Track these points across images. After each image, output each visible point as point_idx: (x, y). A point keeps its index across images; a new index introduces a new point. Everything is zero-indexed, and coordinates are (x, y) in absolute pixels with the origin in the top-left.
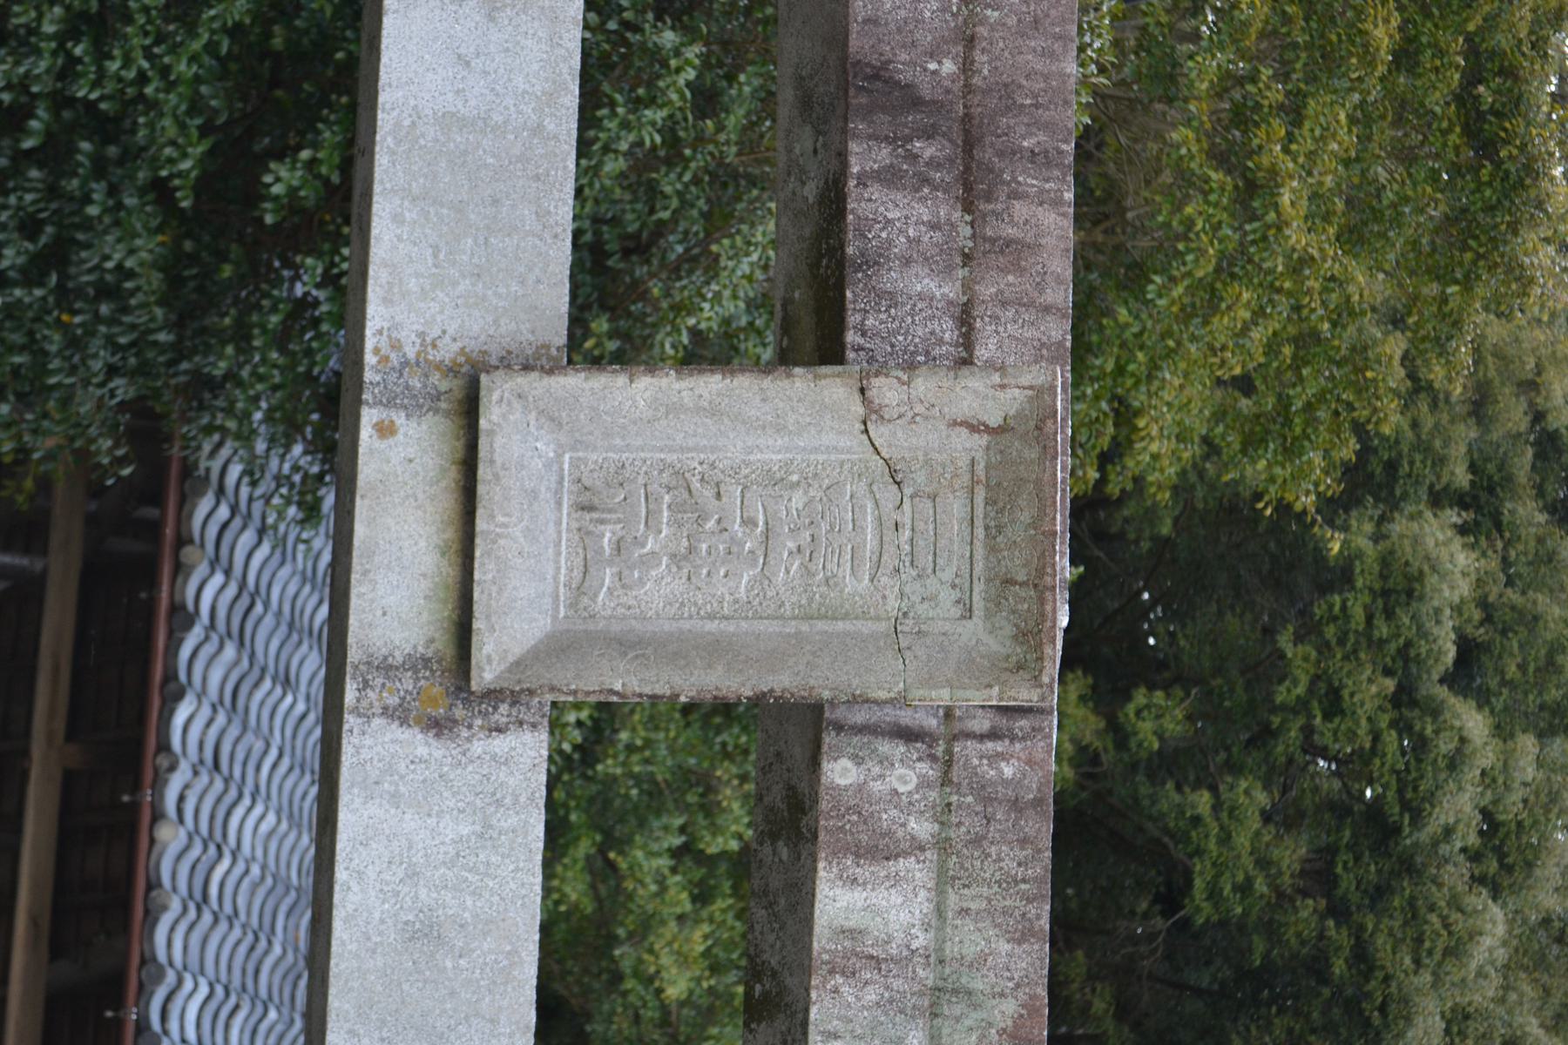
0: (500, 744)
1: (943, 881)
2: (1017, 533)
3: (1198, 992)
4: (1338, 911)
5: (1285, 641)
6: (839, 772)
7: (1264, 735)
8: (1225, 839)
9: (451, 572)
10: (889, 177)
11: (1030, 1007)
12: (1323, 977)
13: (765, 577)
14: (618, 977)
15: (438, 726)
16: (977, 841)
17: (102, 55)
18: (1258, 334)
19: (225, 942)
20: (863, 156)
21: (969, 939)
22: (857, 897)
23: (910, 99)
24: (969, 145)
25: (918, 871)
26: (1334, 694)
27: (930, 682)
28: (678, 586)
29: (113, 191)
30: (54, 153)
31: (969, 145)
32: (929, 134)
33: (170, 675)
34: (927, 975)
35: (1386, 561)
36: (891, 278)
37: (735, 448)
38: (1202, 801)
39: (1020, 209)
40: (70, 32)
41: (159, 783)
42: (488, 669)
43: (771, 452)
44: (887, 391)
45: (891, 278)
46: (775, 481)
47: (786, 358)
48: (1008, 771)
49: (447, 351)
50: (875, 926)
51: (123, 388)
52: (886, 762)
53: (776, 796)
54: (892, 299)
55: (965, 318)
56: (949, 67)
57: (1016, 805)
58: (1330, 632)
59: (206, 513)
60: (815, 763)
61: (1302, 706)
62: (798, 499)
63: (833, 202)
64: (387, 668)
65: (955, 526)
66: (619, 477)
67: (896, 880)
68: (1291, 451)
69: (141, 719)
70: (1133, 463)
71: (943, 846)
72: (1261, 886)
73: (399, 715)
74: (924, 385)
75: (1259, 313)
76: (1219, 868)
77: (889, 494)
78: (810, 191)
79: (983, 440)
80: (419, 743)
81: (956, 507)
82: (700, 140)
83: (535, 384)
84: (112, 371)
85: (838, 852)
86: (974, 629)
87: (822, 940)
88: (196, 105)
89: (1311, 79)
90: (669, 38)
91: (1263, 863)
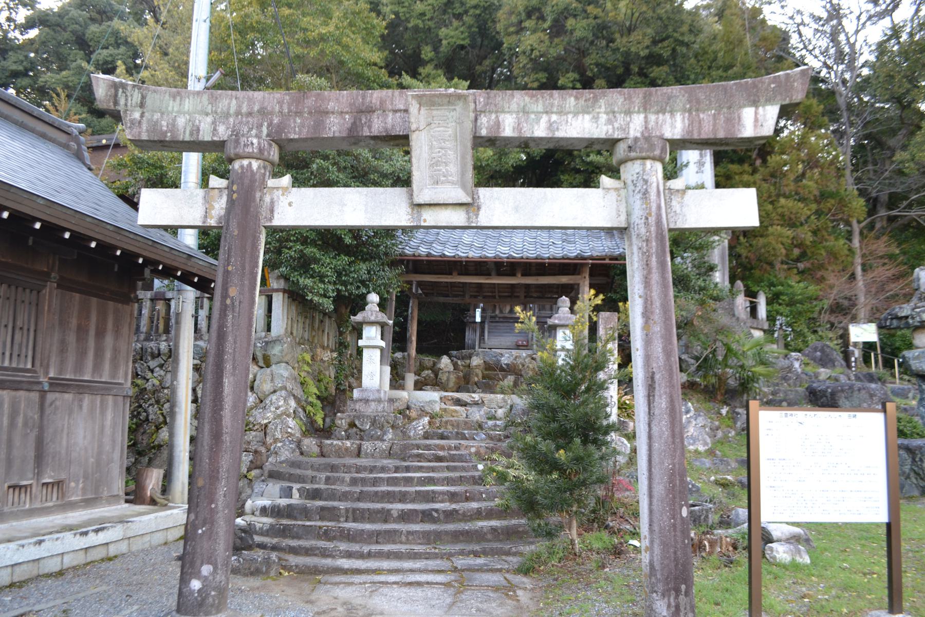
0: (481, 197)
1: (503, 112)
2: (440, 100)
3: (482, 41)
4: (466, 12)
5: (410, 25)
6: (484, 132)
7: (429, 29)
8: (452, 37)
9: (450, 208)
10: (370, 127)
11: (526, 94)
12: (480, 15)
13: (449, 149)
14: (488, 165)
15: (479, 208)
16: (496, 105)
17: (327, 276)
18: (352, 36)
19: (490, 243)
20: (366, 133)
21: (514, 106)
22: (507, 128)
23: (354, 124)
24: (362, 112)
25: (502, 116)
26: (421, 14)
27: (468, 117)
28: (451, 165)
29: (351, 272)
30: (344, 284)
31: (362, 112)
32: (361, 120)
33: (440, 256)
34: (521, 114)
35: (392, 4)
36: (389, 126)
37: (425, 155)
38: (444, 42)
39: (374, 101)
40: (323, 282)
41: (461, 257)
42: (469, 200)
43: (426, 148)
44: (414, 127)
45: (389, 126)
46: (431, 147)
47: (408, 145)
48: (482, 100)
49: (410, 210)
50: (512, 125)
51: (387, 268)
52: (481, 124)
53: (487, 144)
54: (393, 126)
55: (395, 111)
56: (347, 116)
57: (488, 98)
58: (408, 16)
59: (408, 251)
60: (482, 137)
61: (423, 21)
62: (434, 143)
63: (375, 138)
64: (469, 218)
65: (439, 112)
66: (432, 177)
67: (503, 121)
68: (374, 27)
69: (449, 261)
70: (378, 61)
71: (497, 112)
72: (462, 29)
73: (477, 215)
74: (412, 120)
75: (348, 36)
76: (458, 38)
77: (433, 126)
78: (372, 142)
79: (422, 108)
80: (482, 212)
81: (435, 112)
82: (333, 158)
83: (415, 193)
84: (384, 271)
85: (499, 132)
86: (458, 108)
87: (515, 135)
88: (334, 258)
89: (297, 27)
90: (314, 166)
91: (457, 29)
